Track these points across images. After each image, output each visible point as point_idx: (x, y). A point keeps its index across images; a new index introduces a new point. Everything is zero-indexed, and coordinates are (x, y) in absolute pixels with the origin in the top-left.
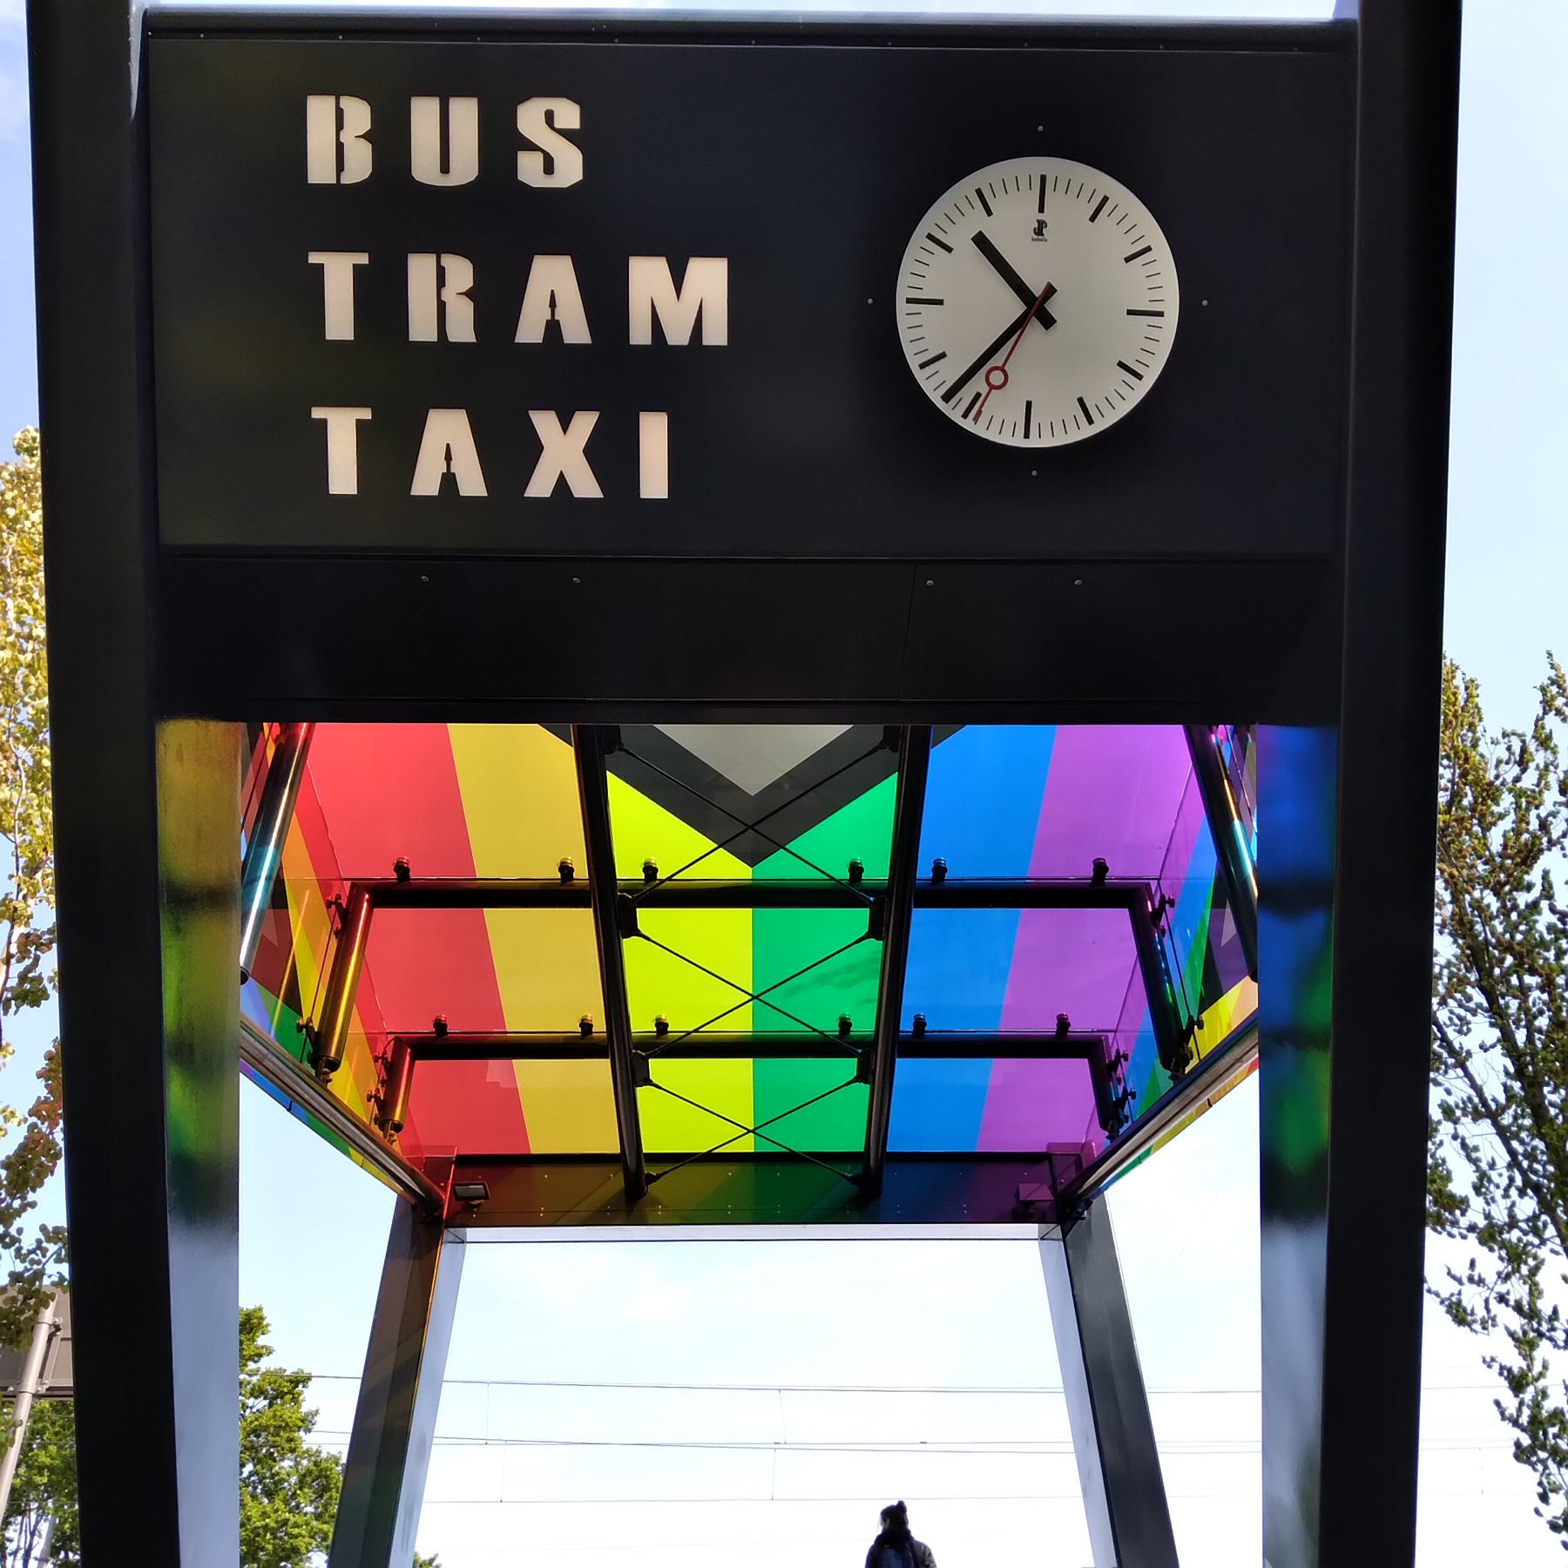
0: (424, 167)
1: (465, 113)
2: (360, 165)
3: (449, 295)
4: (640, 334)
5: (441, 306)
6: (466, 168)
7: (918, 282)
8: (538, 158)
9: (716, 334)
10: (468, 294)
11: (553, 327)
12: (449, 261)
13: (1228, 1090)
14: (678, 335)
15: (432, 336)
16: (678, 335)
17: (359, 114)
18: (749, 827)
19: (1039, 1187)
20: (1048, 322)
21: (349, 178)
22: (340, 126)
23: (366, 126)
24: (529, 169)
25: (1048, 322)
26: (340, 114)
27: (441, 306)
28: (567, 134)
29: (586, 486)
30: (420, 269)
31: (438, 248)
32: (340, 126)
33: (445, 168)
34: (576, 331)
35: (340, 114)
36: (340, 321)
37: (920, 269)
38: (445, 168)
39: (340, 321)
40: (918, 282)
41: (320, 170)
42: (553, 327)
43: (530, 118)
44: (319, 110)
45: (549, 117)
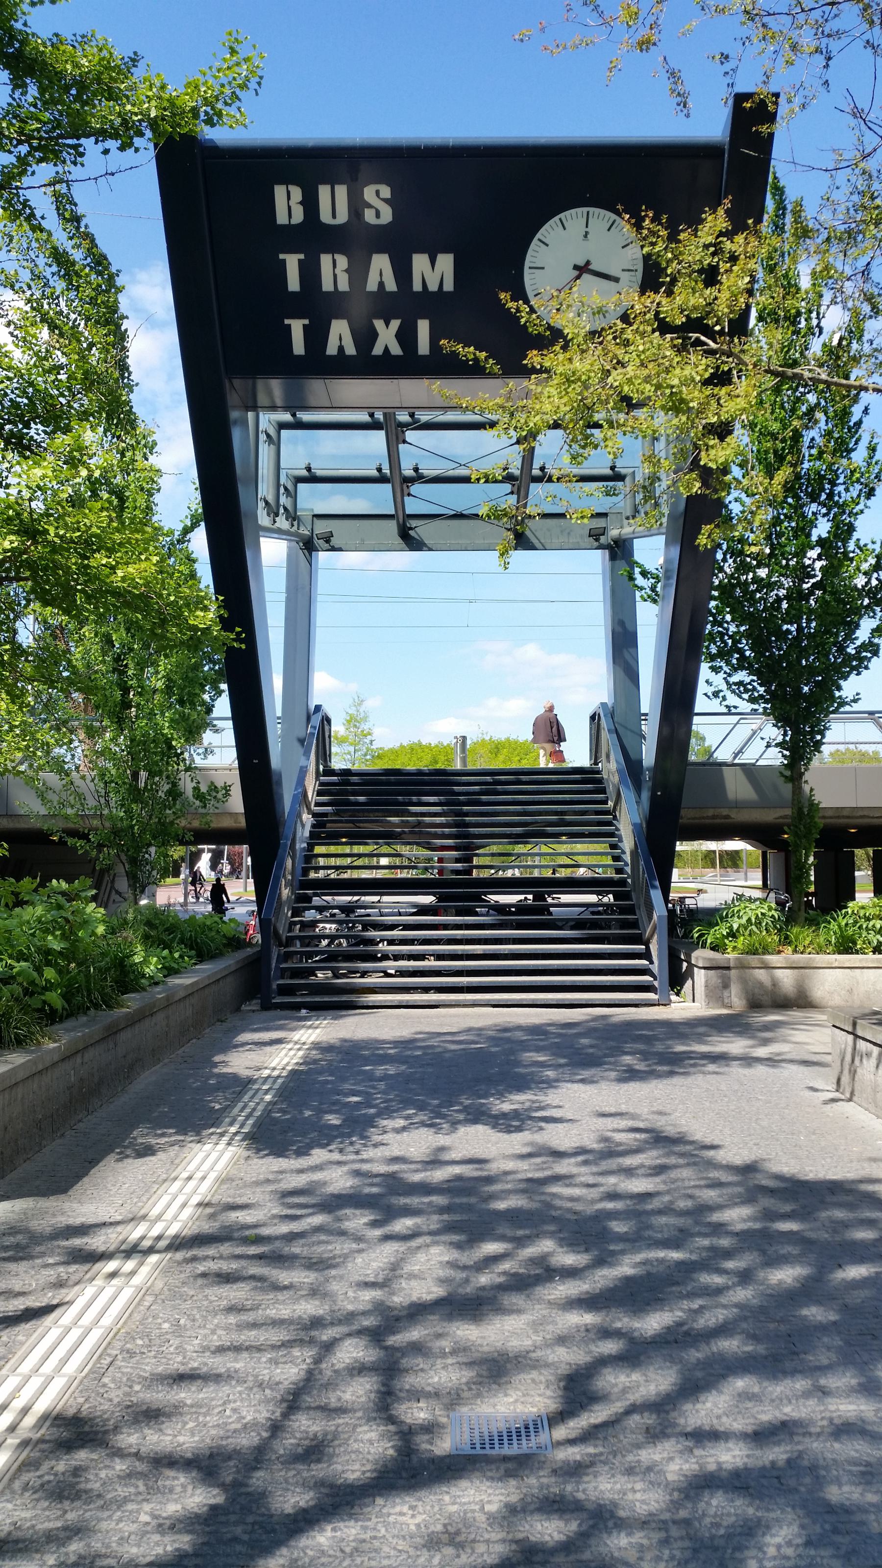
0: (325, 217)
1: (342, 191)
2: (298, 216)
3: (337, 271)
4: (417, 287)
5: (335, 276)
6: (342, 217)
7: (534, 259)
8: (373, 211)
9: (449, 286)
10: (301, 203)
11: (381, 284)
12: (291, 188)
13: (652, 532)
14: (433, 287)
15: (331, 289)
16: (433, 287)
17: (297, 193)
18: (856, 1036)
19: (861, 1181)
20: (588, 263)
21: (293, 222)
22: (289, 198)
23: (300, 198)
24: (369, 216)
25: (588, 263)
26: (288, 193)
27: (335, 276)
28: (385, 200)
29: (396, 350)
30: (326, 260)
31: (286, 182)
32: (289, 198)
33: (334, 216)
34: (391, 286)
35: (288, 193)
36: (294, 284)
37: (535, 254)
38: (334, 216)
39: (294, 284)
40: (534, 259)
41: (282, 218)
42: (381, 284)
43: (369, 194)
44: (280, 191)
45: (377, 193)
